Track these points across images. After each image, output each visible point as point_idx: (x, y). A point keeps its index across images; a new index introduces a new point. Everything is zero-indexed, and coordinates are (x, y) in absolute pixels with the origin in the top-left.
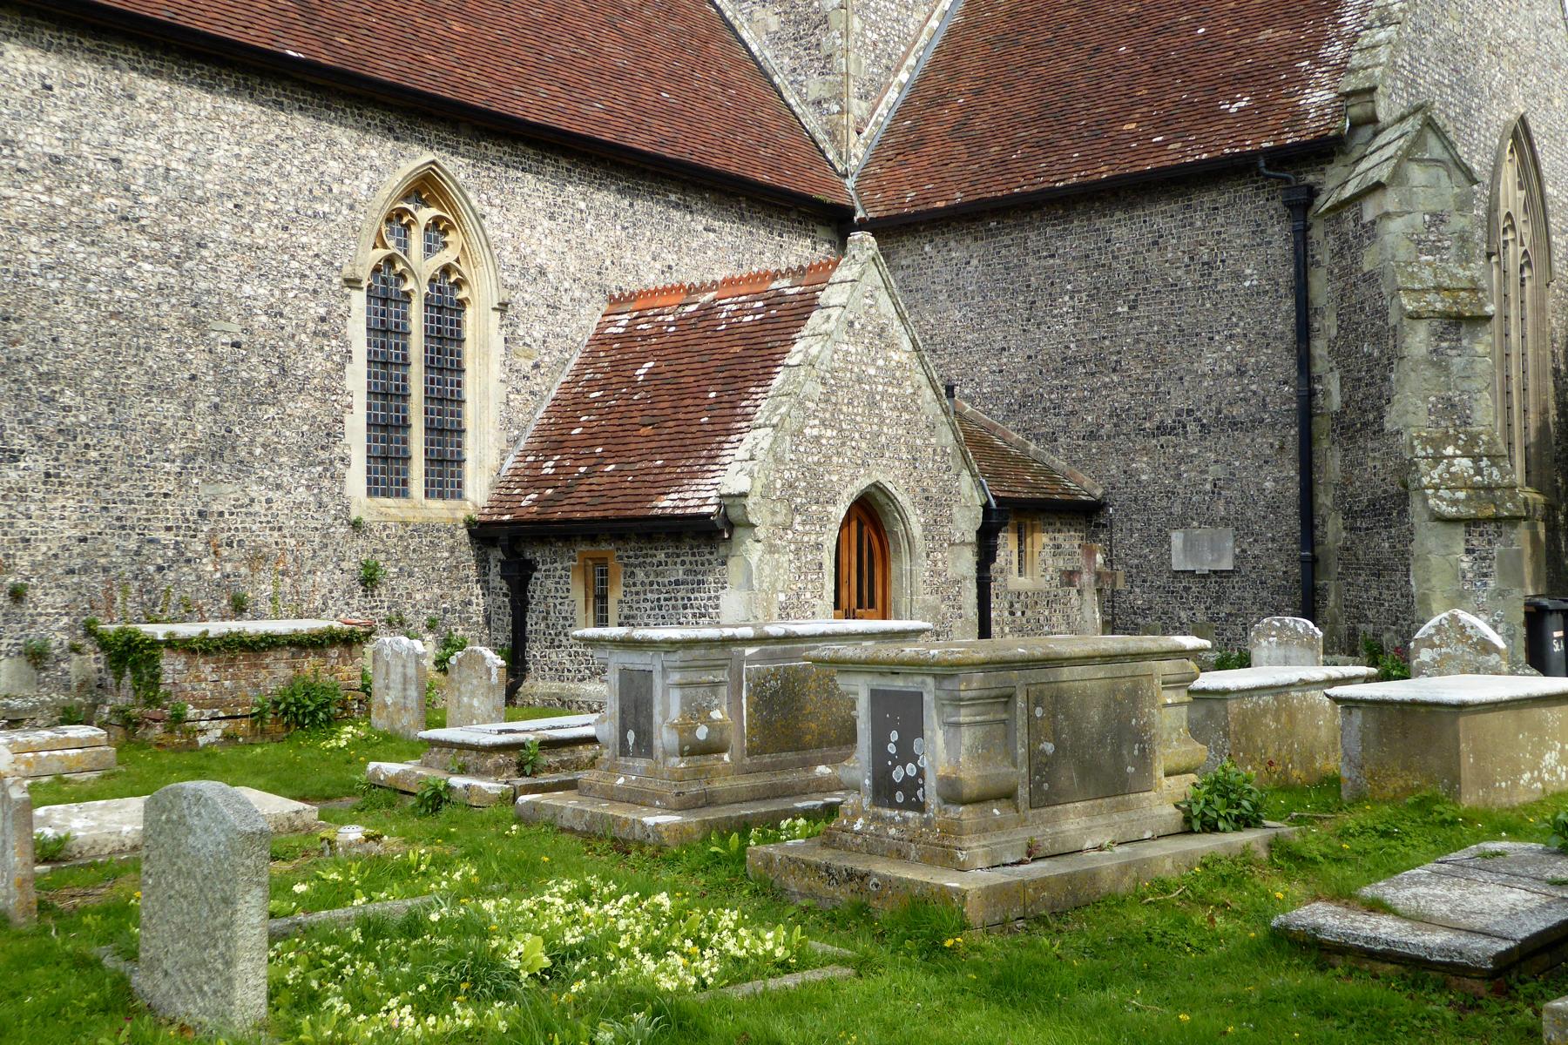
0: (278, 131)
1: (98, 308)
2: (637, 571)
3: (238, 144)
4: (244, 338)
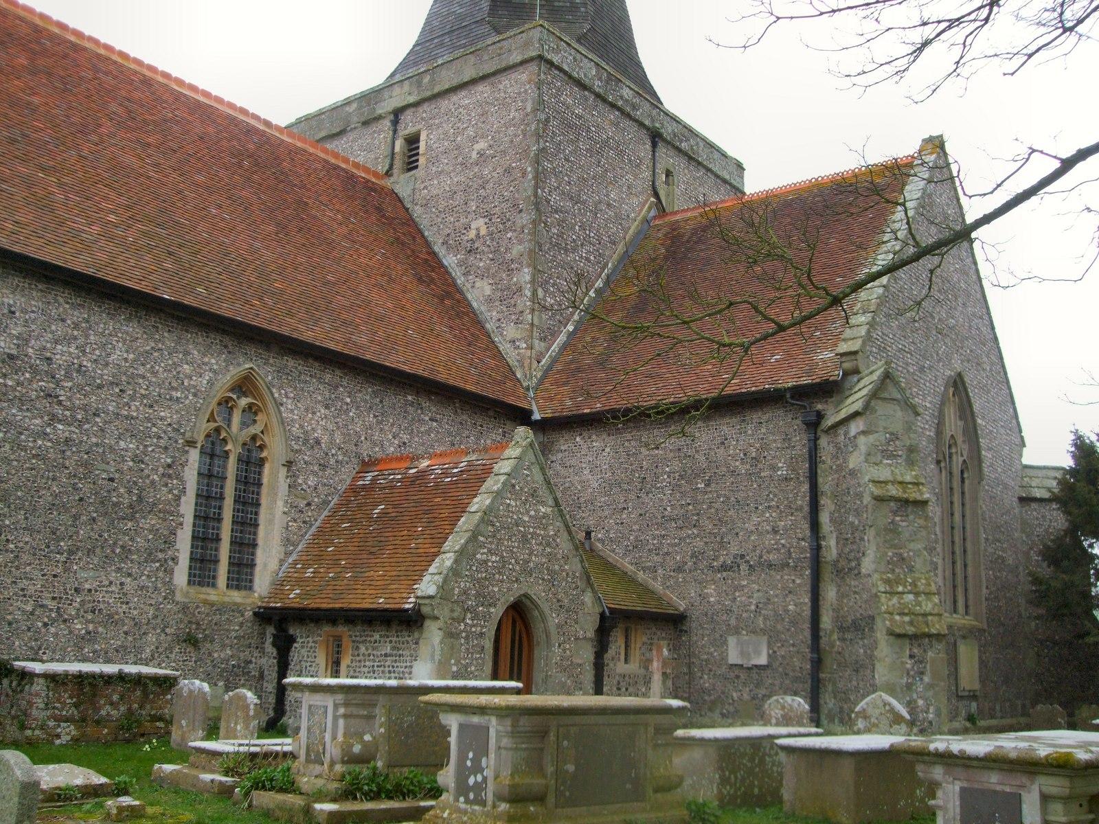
0: (153, 345)
1: (26, 451)
3: (127, 352)
4: (117, 476)
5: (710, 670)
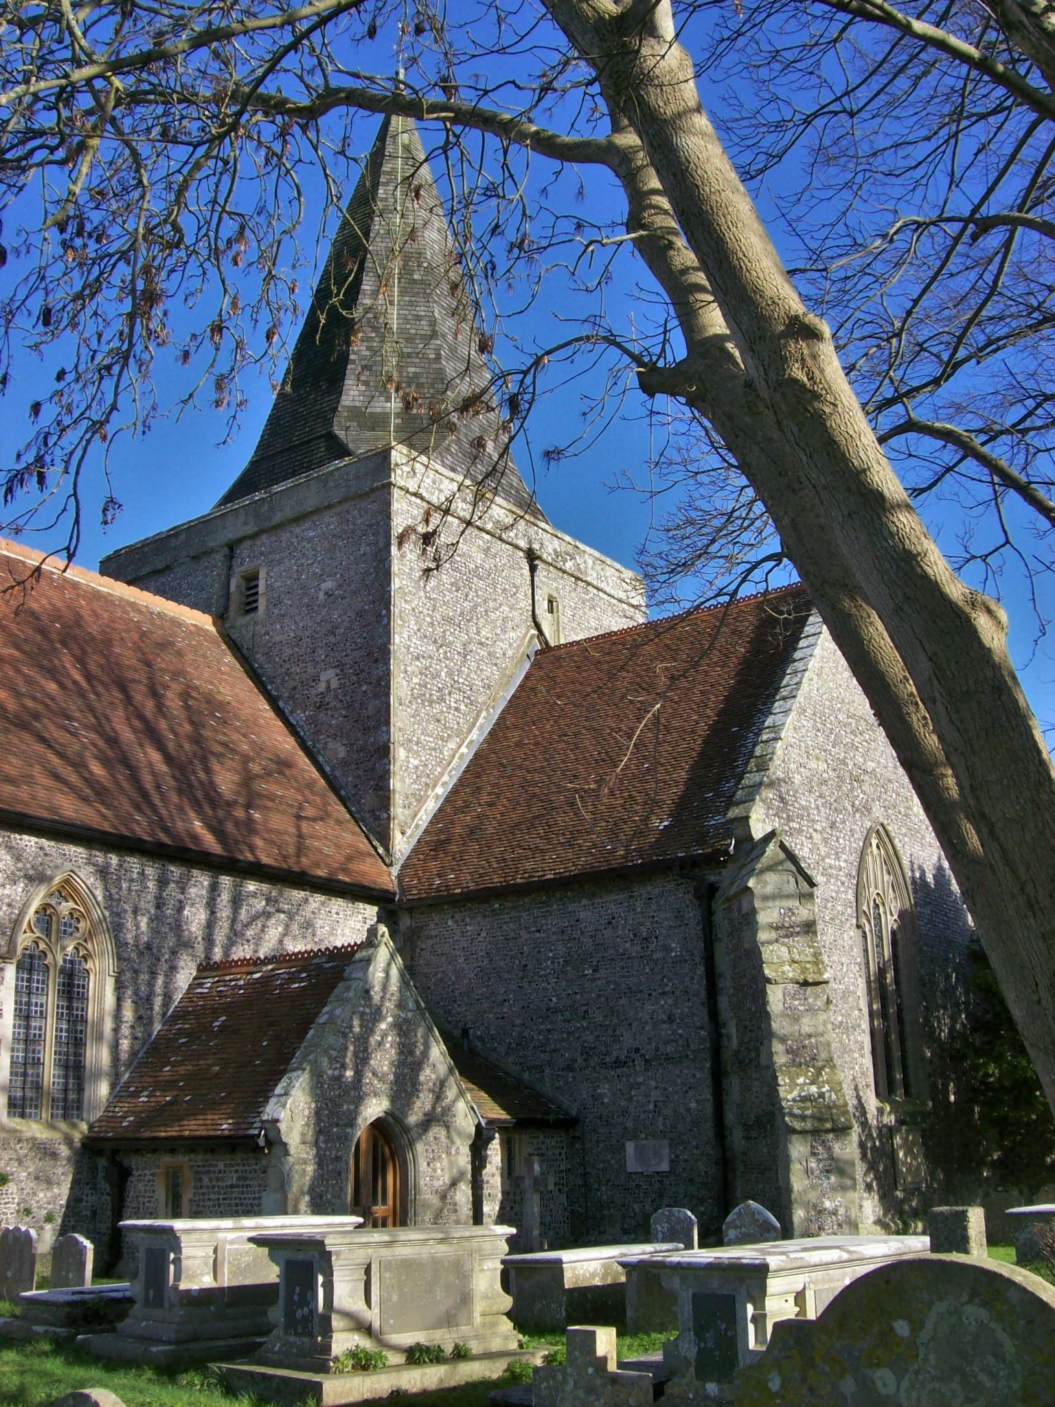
2: (204, 1177)
5: (608, 1181)
